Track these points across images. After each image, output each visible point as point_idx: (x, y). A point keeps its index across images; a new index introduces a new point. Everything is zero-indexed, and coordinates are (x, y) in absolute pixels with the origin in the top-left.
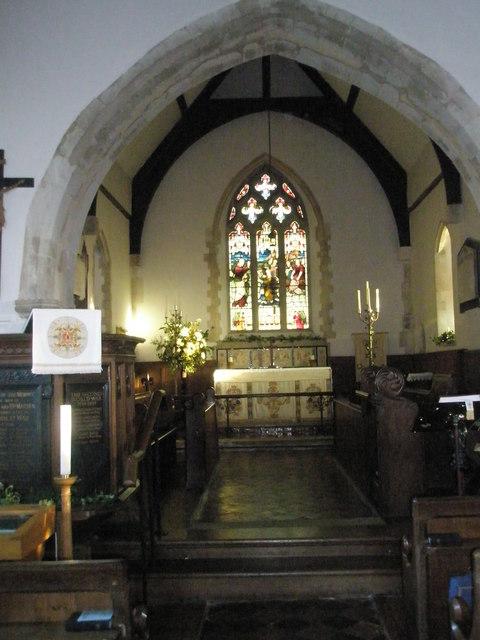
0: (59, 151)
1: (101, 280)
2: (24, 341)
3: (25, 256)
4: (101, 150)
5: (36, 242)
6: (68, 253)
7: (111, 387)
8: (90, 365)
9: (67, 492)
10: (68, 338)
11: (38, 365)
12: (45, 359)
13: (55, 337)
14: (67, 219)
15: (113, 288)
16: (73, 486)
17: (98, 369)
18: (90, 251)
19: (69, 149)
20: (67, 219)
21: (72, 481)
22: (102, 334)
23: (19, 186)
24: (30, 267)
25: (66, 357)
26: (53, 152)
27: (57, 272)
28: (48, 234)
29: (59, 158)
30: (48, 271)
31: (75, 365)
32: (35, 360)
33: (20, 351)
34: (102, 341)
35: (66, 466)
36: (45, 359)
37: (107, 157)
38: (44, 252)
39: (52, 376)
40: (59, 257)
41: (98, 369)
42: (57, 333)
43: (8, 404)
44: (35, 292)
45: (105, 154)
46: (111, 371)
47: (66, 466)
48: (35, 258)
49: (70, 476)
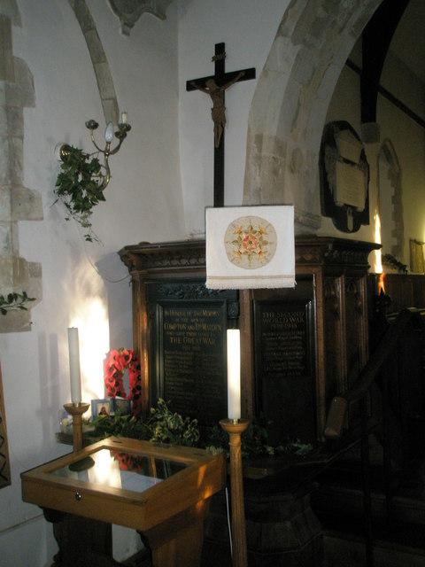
0: (280, 32)
1: (392, 191)
2: (195, 250)
3: (248, 157)
4: (334, 22)
5: (259, 139)
6: (304, 152)
7: (316, 307)
8: (280, 277)
9: (235, 441)
10: (251, 242)
11: (212, 278)
12: (221, 271)
13: (266, 243)
14: (297, 113)
15: (405, 200)
16: (243, 435)
17: (290, 283)
18: (371, 160)
19: (291, 26)
20: (297, 113)
21: (242, 427)
22: (297, 238)
23: (240, 80)
24: (253, 168)
25: (250, 267)
26: (275, 34)
27: (287, 172)
28: (272, 129)
29: (280, 39)
30: (275, 172)
31: (263, 278)
32: (210, 272)
33: (193, 261)
34: (296, 246)
35: (234, 409)
36: (221, 271)
37: (346, 32)
38: (268, 151)
39: (238, 291)
40: (289, 158)
41: (290, 283)
42: (236, 237)
43: (193, 324)
44: (259, 195)
45: (341, 30)
46: (317, 283)
47: (234, 409)
48: (259, 158)
49: (239, 421)
